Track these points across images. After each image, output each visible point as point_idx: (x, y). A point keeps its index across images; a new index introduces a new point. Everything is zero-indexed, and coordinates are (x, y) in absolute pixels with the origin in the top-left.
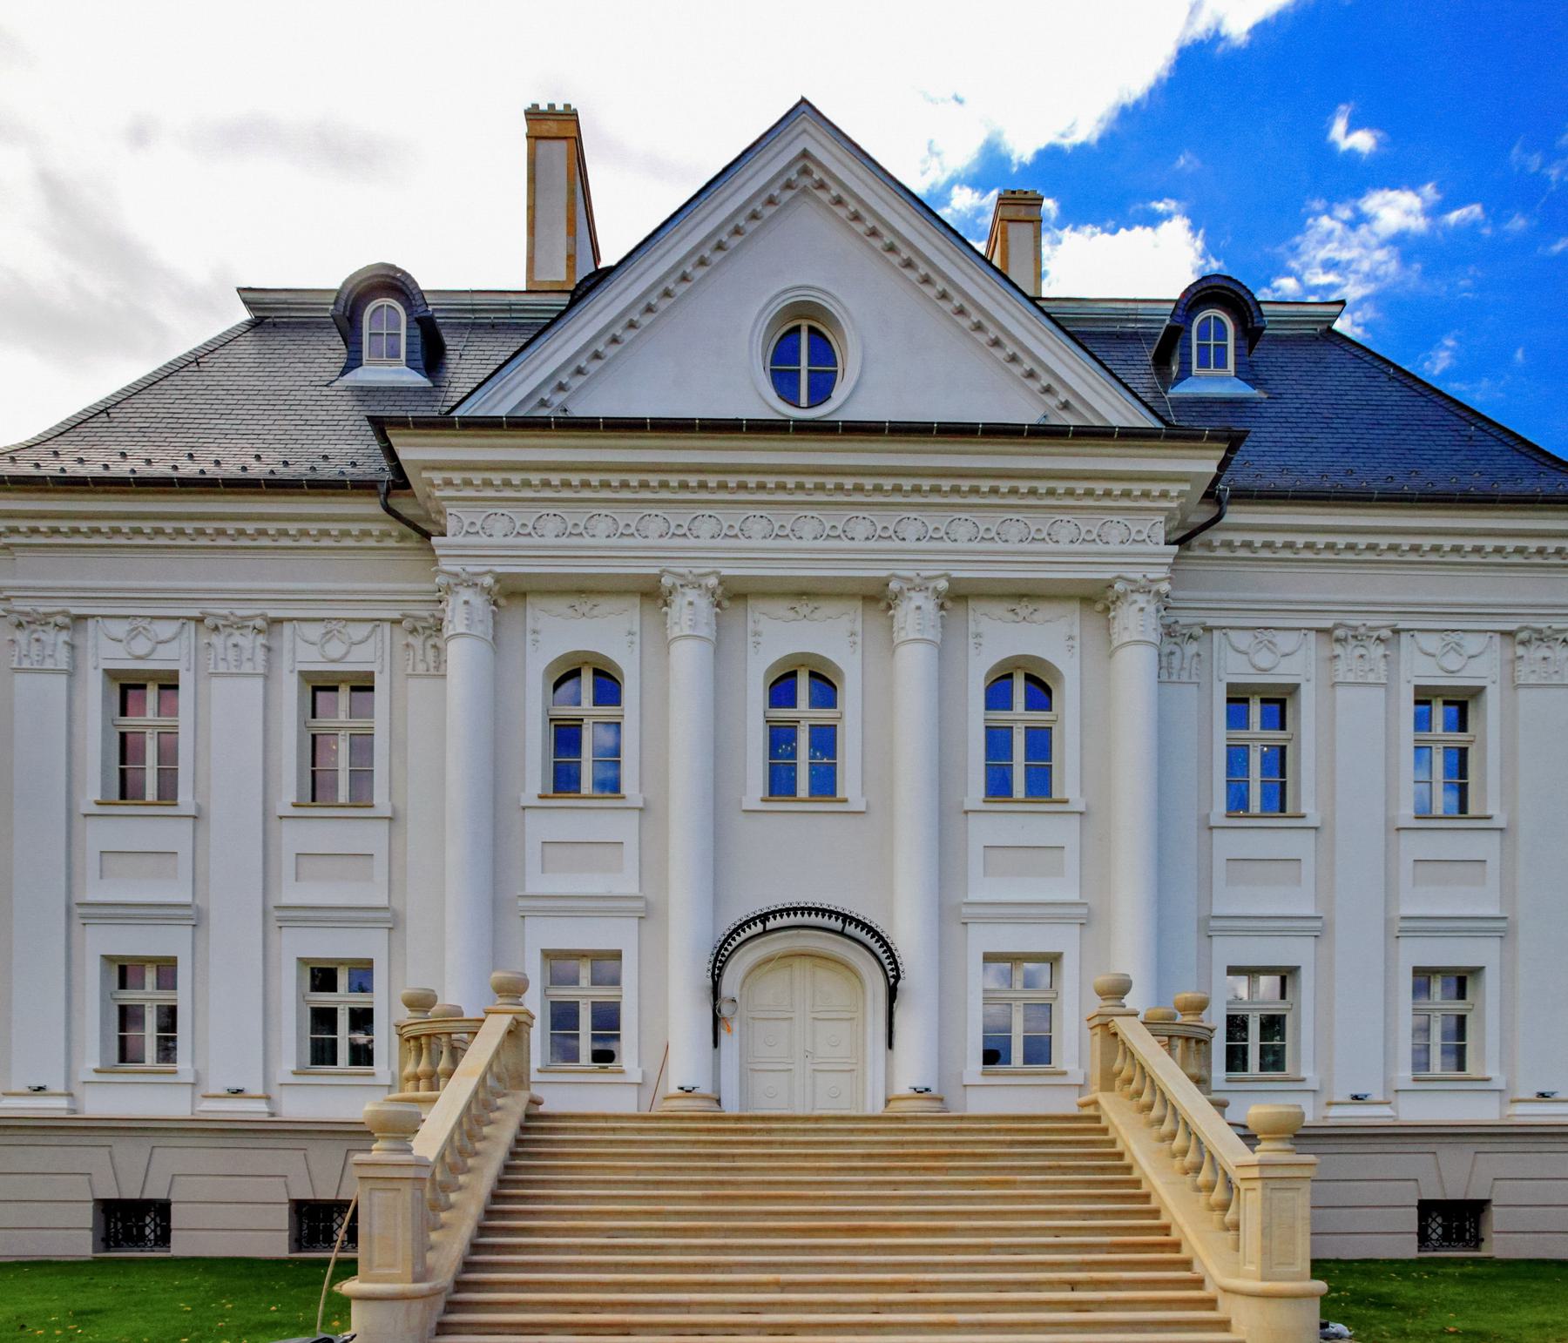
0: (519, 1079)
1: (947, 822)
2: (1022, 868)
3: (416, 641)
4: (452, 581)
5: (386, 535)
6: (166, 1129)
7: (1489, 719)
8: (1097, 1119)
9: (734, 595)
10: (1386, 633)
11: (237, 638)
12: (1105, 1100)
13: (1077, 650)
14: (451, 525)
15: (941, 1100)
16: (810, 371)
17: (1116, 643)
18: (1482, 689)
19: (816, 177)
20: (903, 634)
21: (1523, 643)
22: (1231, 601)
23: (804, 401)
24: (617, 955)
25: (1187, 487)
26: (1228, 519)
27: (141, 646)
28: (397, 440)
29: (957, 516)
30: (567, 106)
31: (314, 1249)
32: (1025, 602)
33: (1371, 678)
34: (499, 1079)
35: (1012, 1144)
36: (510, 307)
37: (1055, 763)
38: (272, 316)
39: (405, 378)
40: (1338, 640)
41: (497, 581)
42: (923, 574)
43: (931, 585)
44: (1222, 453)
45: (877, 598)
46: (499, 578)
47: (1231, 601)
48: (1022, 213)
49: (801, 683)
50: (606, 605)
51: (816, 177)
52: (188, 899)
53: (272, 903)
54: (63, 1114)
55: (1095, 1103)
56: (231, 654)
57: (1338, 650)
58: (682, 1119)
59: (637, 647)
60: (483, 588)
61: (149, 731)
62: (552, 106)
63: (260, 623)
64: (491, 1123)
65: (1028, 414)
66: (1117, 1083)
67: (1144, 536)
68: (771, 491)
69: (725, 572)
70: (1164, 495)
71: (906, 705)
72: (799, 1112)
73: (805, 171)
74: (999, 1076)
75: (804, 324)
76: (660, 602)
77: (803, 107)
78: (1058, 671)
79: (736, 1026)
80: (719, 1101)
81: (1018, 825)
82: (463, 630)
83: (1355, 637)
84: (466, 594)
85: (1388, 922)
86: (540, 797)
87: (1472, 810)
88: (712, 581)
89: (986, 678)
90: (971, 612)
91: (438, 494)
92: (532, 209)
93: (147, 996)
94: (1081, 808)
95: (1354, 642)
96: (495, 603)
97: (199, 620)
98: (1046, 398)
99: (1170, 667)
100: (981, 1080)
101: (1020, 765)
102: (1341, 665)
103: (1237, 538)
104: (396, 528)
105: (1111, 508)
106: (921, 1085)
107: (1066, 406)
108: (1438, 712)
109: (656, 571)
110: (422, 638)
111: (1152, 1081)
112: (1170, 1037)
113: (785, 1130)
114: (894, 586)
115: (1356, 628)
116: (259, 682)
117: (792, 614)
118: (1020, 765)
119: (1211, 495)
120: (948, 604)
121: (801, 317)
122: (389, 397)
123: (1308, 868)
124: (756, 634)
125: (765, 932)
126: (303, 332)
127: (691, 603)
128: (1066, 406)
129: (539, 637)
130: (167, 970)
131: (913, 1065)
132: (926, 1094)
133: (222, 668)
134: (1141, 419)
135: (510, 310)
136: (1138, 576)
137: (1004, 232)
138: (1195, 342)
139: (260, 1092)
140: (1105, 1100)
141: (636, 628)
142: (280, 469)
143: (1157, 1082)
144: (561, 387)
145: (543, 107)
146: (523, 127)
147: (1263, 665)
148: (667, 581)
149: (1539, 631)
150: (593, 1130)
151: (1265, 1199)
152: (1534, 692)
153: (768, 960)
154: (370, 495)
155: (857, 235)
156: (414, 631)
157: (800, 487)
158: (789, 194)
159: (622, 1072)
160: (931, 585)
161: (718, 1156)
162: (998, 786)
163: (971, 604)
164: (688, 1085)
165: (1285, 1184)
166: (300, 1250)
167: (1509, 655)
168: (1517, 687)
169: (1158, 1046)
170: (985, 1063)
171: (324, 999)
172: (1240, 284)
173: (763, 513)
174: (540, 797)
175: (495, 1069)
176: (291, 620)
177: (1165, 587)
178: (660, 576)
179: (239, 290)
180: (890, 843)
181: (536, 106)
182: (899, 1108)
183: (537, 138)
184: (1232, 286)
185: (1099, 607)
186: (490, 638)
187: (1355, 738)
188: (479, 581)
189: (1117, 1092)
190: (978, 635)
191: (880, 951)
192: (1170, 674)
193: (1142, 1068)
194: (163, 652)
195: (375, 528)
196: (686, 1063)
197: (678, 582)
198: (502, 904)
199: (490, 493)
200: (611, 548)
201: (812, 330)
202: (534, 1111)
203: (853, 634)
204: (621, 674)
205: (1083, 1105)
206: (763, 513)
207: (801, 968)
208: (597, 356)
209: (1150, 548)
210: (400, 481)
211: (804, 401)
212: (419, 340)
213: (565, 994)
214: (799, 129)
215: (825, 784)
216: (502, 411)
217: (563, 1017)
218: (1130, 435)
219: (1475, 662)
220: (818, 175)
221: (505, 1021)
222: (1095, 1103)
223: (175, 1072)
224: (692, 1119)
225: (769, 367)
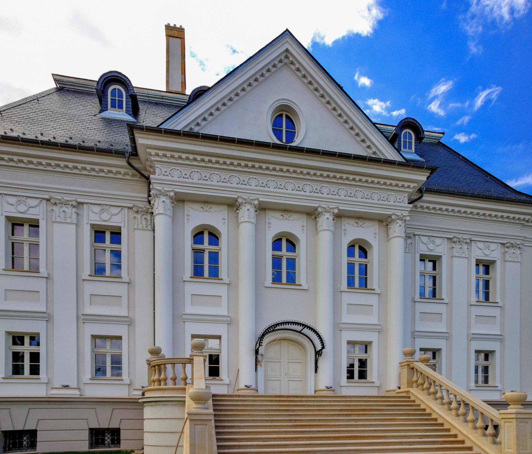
1: (336, 293)
2: (360, 313)
3: (139, 216)
4: (158, 193)
5: (126, 174)
6: (109, 402)
7: (497, 272)
8: (409, 397)
9: (263, 208)
10: (468, 241)
11: (64, 208)
14: (157, 171)
18: (495, 261)
20: (322, 227)
21: (507, 247)
22: (423, 226)
25: (416, 185)
26: (424, 198)
27: (22, 208)
28: (137, 135)
29: (323, 185)
30: (181, 26)
31: (98, 447)
32: (361, 220)
33: (464, 255)
36: (162, 97)
38: (66, 87)
39: (125, 117)
40: (454, 242)
43: (332, 211)
44: (428, 174)
46: (176, 193)
47: (423, 226)
49: (285, 242)
50: (295, 216)
52: (44, 310)
53: (80, 314)
54: (78, 396)
56: (62, 214)
57: (454, 245)
61: (25, 242)
62: (175, 25)
63: (74, 203)
67: (401, 201)
68: (277, 171)
70: (408, 187)
71: (321, 252)
72: (283, 394)
77: (287, 32)
78: (370, 244)
79: (263, 364)
82: (162, 212)
83: (459, 241)
84: (163, 198)
85: (468, 335)
87: (491, 299)
88: (256, 202)
89: (348, 244)
91: (152, 158)
92: (168, 62)
93: (26, 349)
95: (458, 243)
97: (48, 200)
100: (347, 384)
101: (359, 278)
102: (455, 250)
103: (425, 205)
104: (131, 171)
106: (329, 385)
108: (481, 268)
109: (236, 197)
110: (140, 215)
115: (459, 238)
116: (74, 227)
117: (282, 217)
118: (359, 278)
119: (420, 191)
121: (283, 111)
122: (119, 122)
123: (444, 317)
126: (81, 95)
127: (248, 210)
128: (375, 153)
129: (190, 218)
130: (34, 339)
131: (325, 379)
132: (331, 389)
133: (58, 220)
135: (162, 99)
136: (400, 214)
138: (402, 140)
139: (76, 386)
141: (226, 218)
142: (81, 143)
144: (198, 124)
145: (172, 25)
147: (432, 248)
149: (512, 244)
151: (517, 426)
152: (511, 263)
153: (274, 341)
154: (121, 157)
156: (137, 212)
157: (288, 171)
158: (281, 64)
159: (222, 380)
160: (253, 202)
164: (248, 384)
165: (523, 420)
166: (91, 448)
167: (503, 251)
168: (505, 261)
171: (18, 348)
172: (416, 121)
173: (274, 179)
176: (87, 203)
178: (238, 198)
179: (53, 75)
180: (318, 299)
181: (169, 24)
182: (318, 394)
183: (169, 36)
184: (415, 122)
185: (385, 224)
187: (459, 275)
188: (168, 194)
190: (345, 230)
194: (32, 211)
195: (123, 171)
196: (246, 378)
197: (244, 201)
198: (177, 317)
200: (219, 186)
201: (287, 116)
206: (274, 179)
207: (285, 344)
209: (403, 204)
210: (135, 153)
212: (130, 103)
214: (285, 41)
215: (291, 279)
216: (178, 128)
219: (493, 253)
223: (39, 379)
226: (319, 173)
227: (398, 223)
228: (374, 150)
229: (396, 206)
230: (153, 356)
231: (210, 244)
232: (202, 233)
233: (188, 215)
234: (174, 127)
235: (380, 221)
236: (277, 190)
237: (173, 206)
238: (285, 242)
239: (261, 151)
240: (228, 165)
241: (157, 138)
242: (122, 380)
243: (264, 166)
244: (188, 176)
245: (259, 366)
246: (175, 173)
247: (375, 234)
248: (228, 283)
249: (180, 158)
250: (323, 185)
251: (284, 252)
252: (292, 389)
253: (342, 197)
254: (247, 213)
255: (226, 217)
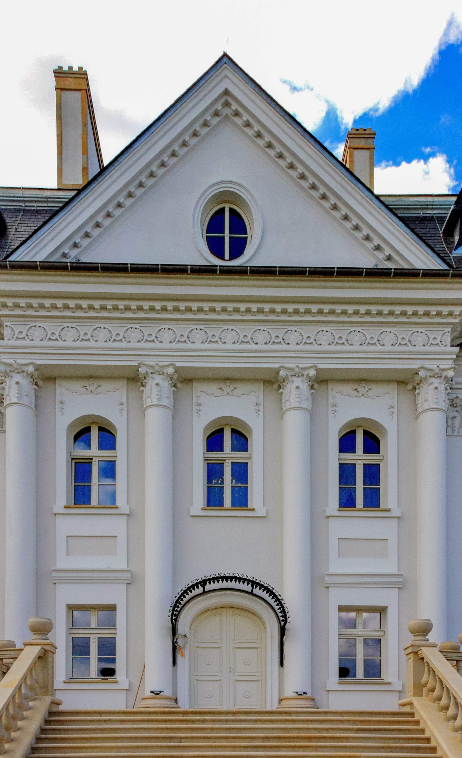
0: (46, 687)
1: (315, 523)
2: (361, 547)
4: (8, 369)
8: (412, 715)
9: (185, 380)
12: (416, 701)
13: (395, 415)
15: (313, 700)
16: (230, 238)
17: (420, 410)
19: (233, 108)
20: (149, 400)
23: (227, 256)
24: (112, 608)
29: (321, 329)
30: (80, 68)
34: (31, 688)
35: (358, 730)
37: (382, 486)
41: (37, 370)
42: (300, 366)
43: (305, 373)
45: (272, 382)
46: (38, 368)
48: (362, 143)
49: (363, 439)
50: (107, 386)
51: (233, 108)
55: (411, 704)
58: (150, 713)
59: (125, 412)
60: (28, 374)
64: (24, 718)
65: (366, 261)
66: (424, 690)
67: (438, 341)
68: (206, 313)
69: (178, 364)
70: (451, 314)
71: (290, 457)
72: (225, 708)
73: (227, 104)
74: (349, 685)
75: (227, 207)
76: (139, 384)
79: (187, 652)
80: (176, 701)
81: (360, 525)
84: (17, 377)
86: (65, 507)
88: (171, 370)
90: (330, 391)
94: (399, 515)
96: (36, 384)
98: (377, 253)
99: (453, 426)
105: (416, 323)
107: (389, 258)
109: (136, 364)
111: (448, 690)
112: (458, 661)
113: (214, 720)
114: (282, 373)
117: (220, 392)
120: (316, 386)
121: (224, 202)
124: (198, 405)
125: (204, 593)
127: (157, 384)
128: (389, 258)
129: (201, 408)
131: (295, 677)
132: (303, 696)
134: (436, 264)
136: (434, 367)
137: (351, 156)
140: (416, 701)
141: (124, 400)
143: (451, 691)
144: (76, 245)
145: (65, 68)
146: (52, 82)
148: (142, 370)
150: (92, 721)
155: (259, 146)
157: (224, 310)
158: (217, 119)
160: (305, 373)
161: (170, 739)
162: (347, 501)
163: (330, 386)
164: (157, 690)
169: (451, 666)
170: (340, 676)
173: (202, 327)
174: (65, 507)
175: (28, 682)
177: (451, 374)
178: (139, 367)
181: (60, 68)
182: (288, 705)
183: (62, 89)
185: (410, 387)
186: (33, 406)
188: (25, 369)
189: (425, 697)
190: (334, 405)
191: (277, 608)
192: (453, 431)
193: (441, 681)
196: (156, 676)
199: (31, 312)
202: (55, 709)
203: (257, 405)
204: (116, 432)
205: (403, 705)
206: (202, 327)
207: (228, 618)
208: (98, 225)
209: (441, 348)
211: (227, 256)
213: (81, 632)
214: (223, 75)
216: (40, 258)
217: (80, 648)
218: (430, 274)
220: (234, 106)
221: (34, 651)
222: (411, 704)
224: (155, 713)
225: (205, 234)
226: (398, 309)
227: (432, 383)
228: (388, 251)
229: (399, 353)
230: (417, 638)
231: (101, 447)
232: (87, 430)
233: (61, 403)
234: (33, 257)
235: (401, 383)
236: (206, 346)
237: (174, 391)
238: (224, 437)
239: (324, 284)
240: (182, 312)
241: (92, 279)
242: (116, 682)
243: (182, 306)
244: (153, 337)
245: (179, 657)
246: (36, 333)
247: (392, 407)
248: (128, 512)
249: (79, 307)
250: (321, 329)
251: (94, 451)
252: (244, 698)
253: (325, 347)
254: (296, 392)
255: (261, 400)
